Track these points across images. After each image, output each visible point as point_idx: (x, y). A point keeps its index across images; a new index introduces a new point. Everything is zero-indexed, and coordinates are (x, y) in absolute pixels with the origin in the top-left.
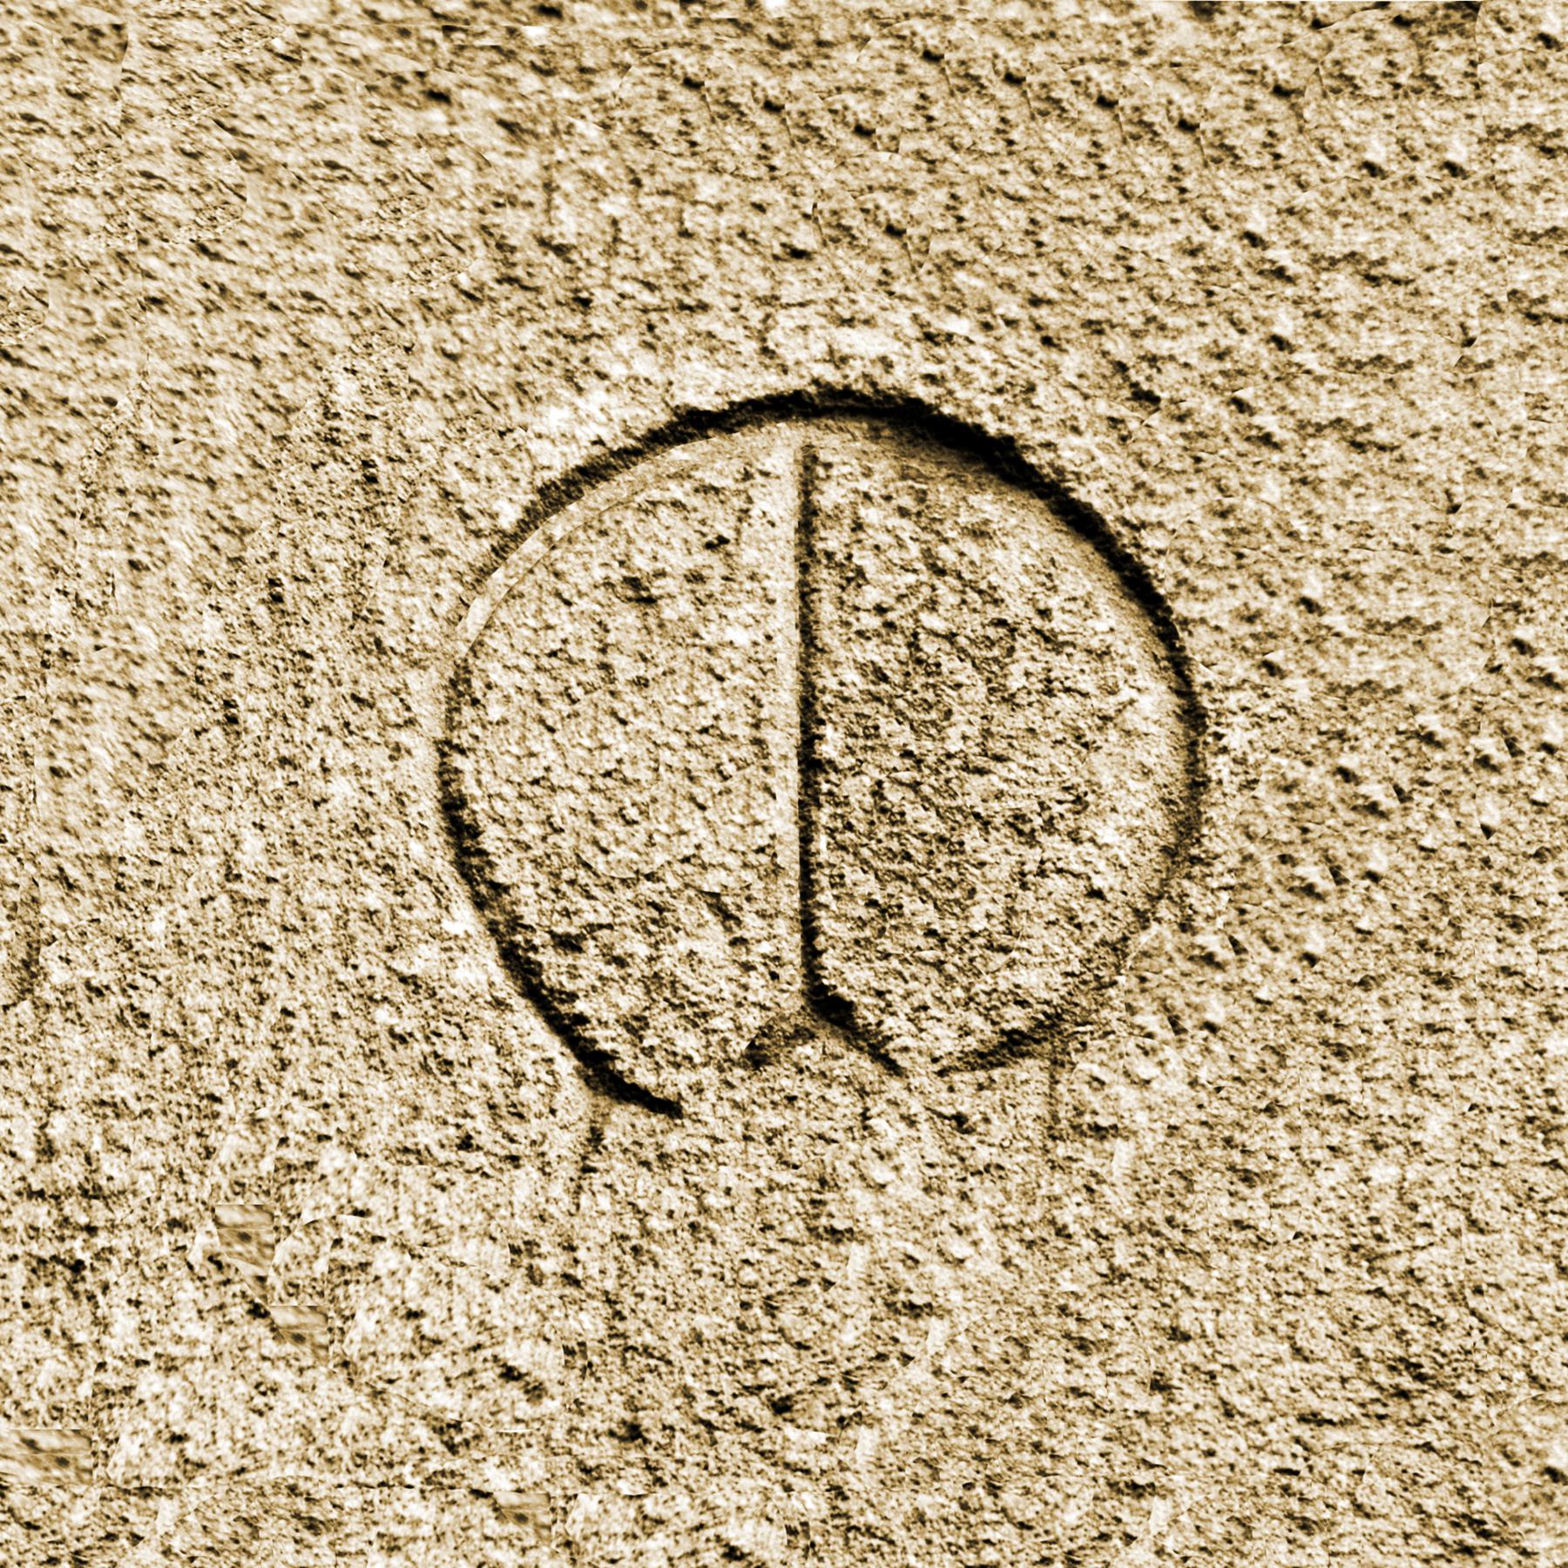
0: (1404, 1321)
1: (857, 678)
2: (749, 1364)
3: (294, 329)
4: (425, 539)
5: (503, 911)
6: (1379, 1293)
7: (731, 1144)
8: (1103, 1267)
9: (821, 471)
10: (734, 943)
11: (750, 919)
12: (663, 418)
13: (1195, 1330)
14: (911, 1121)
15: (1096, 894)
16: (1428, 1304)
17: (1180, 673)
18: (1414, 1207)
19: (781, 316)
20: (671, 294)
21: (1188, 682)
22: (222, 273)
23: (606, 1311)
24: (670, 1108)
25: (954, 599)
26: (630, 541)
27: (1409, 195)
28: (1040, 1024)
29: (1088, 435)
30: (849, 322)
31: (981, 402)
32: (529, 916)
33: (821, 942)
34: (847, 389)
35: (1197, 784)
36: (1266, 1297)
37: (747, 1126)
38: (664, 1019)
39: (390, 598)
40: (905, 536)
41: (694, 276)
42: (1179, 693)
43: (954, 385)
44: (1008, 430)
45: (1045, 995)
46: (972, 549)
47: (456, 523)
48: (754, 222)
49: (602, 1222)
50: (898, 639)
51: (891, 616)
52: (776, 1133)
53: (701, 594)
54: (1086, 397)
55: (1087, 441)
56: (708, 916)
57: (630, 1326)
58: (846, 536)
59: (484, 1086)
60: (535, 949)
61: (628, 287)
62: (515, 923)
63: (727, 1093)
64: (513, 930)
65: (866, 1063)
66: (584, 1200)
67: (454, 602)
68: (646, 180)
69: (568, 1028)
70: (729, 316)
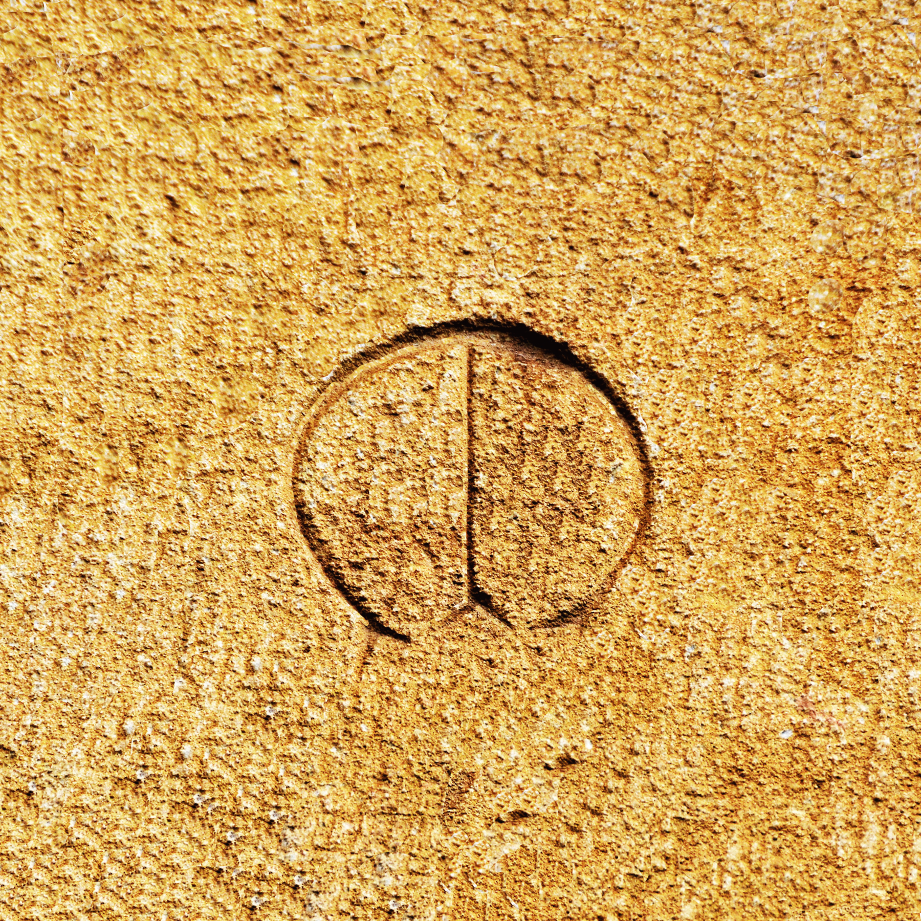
0: (736, 749)
1: (494, 451)
2: (438, 752)
3: (218, 283)
4: (284, 385)
5: (325, 551)
6: (726, 736)
7: (433, 656)
8: (601, 720)
9: (477, 356)
10: (436, 567)
11: (444, 558)
12: (402, 330)
13: (641, 750)
14: (516, 649)
15: (603, 551)
16: (748, 741)
17: (642, 452)
18: (743, 697)
19: (458, 282)
20: (406, 270)
21: (646, 457)
22: (183, 253)
23: (373, 724)
24: (406, 639)
25: (539, 417)
26: (386, 387)
27: (757, 229)
28: (576, 608)
29: (602, 342)
30: (490, 286)
31: (552, 326)
32: (338, 554)
33: (476, 569)
34: (490, 318)
35: (649, 502)
36: (674, 737)
37: (441, 648)
38: (402, 600)
39: (266, 414)
40: (517, 387)
41: (416, 262)
42: (642, 461)
43: (540, 318)
44: (565, 339)
45: (579, 595)
46: (548, 394)
47: (300, 379)
48: (446, 236)
49: (372, 686)
50: (513, 434)
51: (510, 424)
52: (454, 651)
53: (421, 412)
54: (602, 324)
55: (602, 345)
56: (424, 555)
57: (384, 731)
58: (489, 387)
59: (316, 626)
60: (341, 568)
61: (385, 266)
62: (331, 557)
63: (432, 633)
64: (330, 560)
65: (496, 621)
66: (364, 676)
67: (299, 415)
68: (393, 213)
69: (358, 603)
70: (433, 281)
